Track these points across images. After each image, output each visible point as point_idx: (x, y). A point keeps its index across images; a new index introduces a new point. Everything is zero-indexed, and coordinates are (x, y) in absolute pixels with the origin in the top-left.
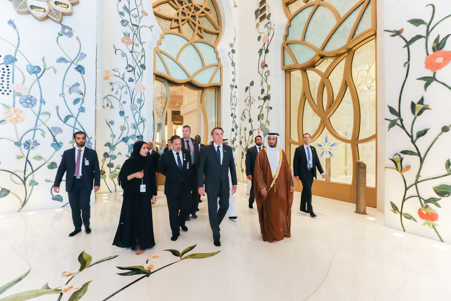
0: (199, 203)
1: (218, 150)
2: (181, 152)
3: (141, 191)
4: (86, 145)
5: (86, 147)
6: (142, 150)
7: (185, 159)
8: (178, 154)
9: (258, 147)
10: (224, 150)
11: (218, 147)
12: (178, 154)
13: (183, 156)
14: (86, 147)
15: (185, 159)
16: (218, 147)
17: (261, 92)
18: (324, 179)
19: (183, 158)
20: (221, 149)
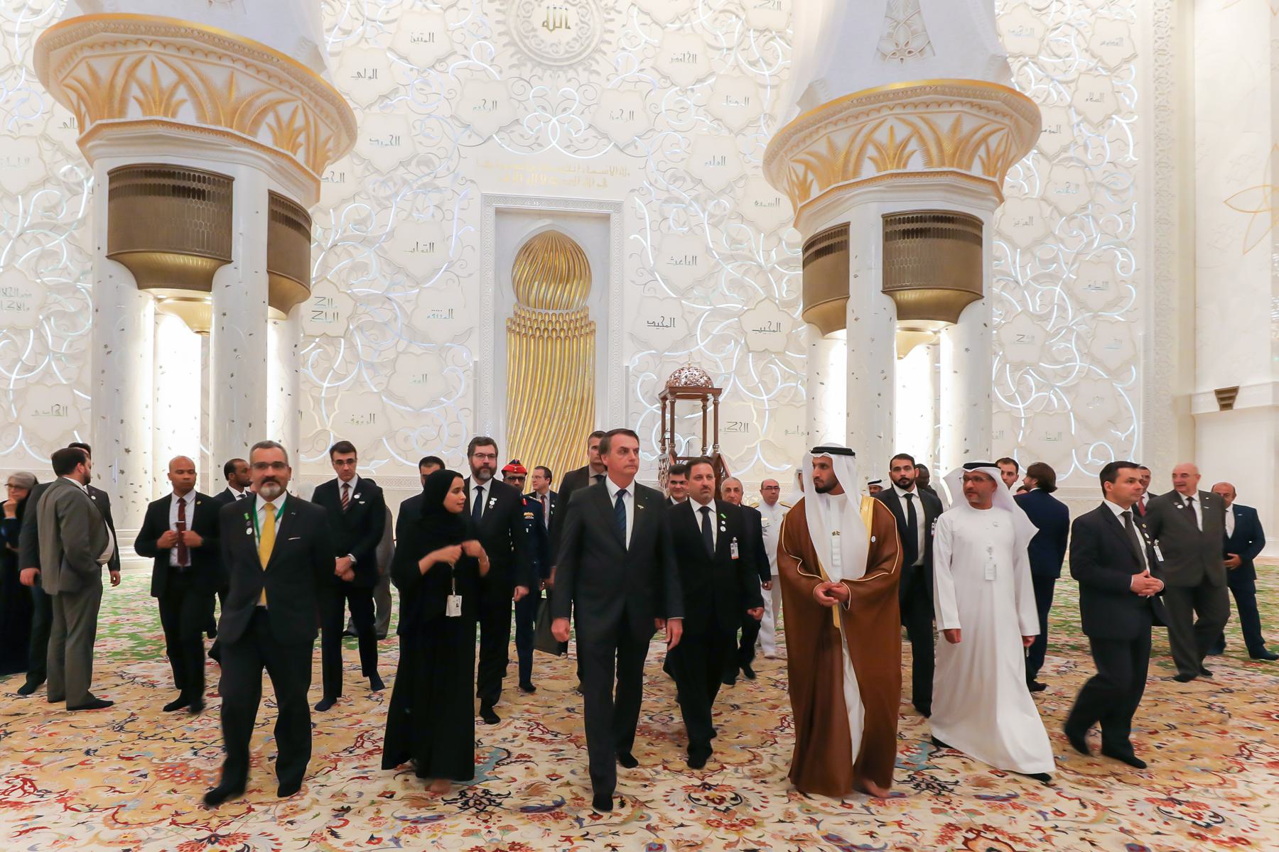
0: (723, 686)
1: (620, 502)
2: (712, 505)
3: (1095, 672)
4: (197, 488)
5: (636, 484)
6: (450, 495)
7: (723, 529)
8: (705, 511)
9: (900, 493)
10: (1203, 504)
11: (621, 493)
12: (705, 511)
13: (719, 519)
14: (636, 484)
15: (723, 529)
16: (621, 493)
17: (790, 280)
18: (564, 627)
19: (719, 525)
20: (629, 502)
